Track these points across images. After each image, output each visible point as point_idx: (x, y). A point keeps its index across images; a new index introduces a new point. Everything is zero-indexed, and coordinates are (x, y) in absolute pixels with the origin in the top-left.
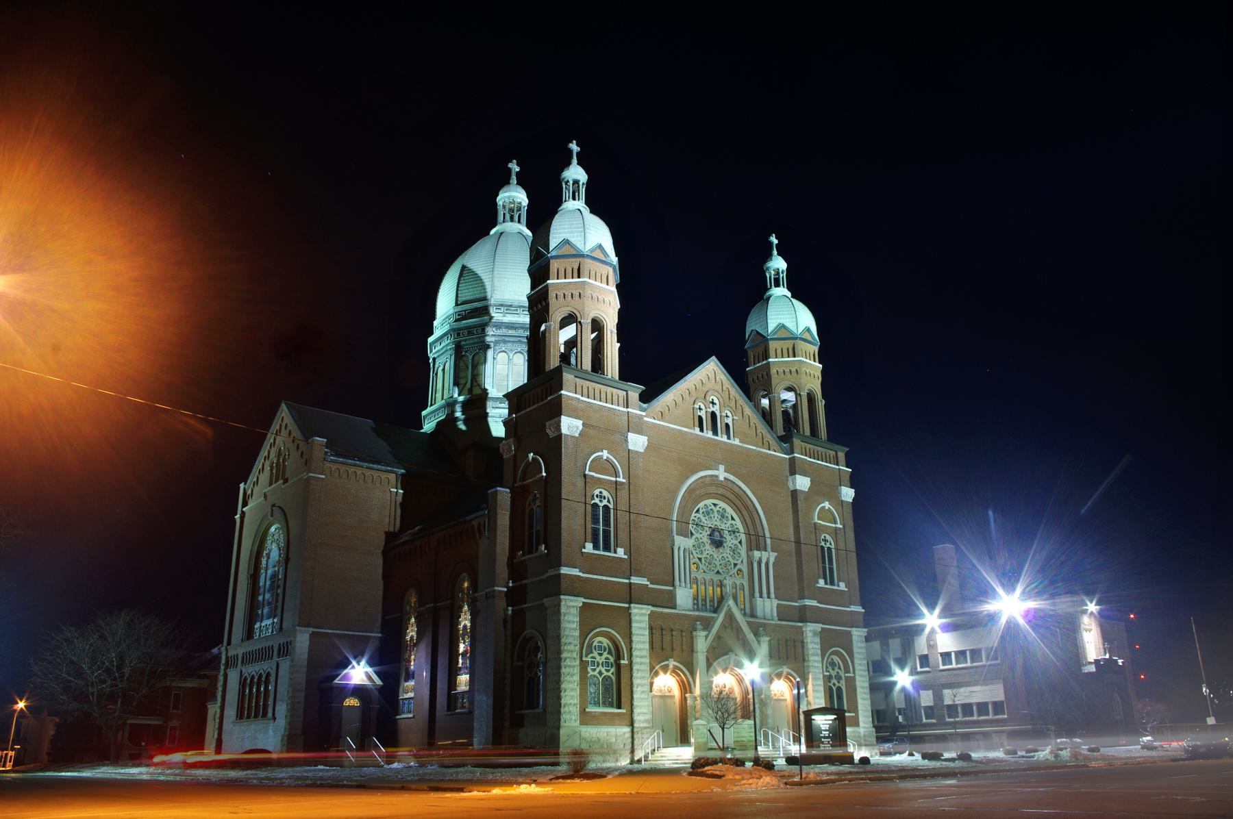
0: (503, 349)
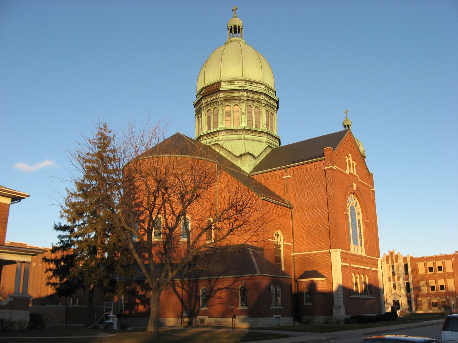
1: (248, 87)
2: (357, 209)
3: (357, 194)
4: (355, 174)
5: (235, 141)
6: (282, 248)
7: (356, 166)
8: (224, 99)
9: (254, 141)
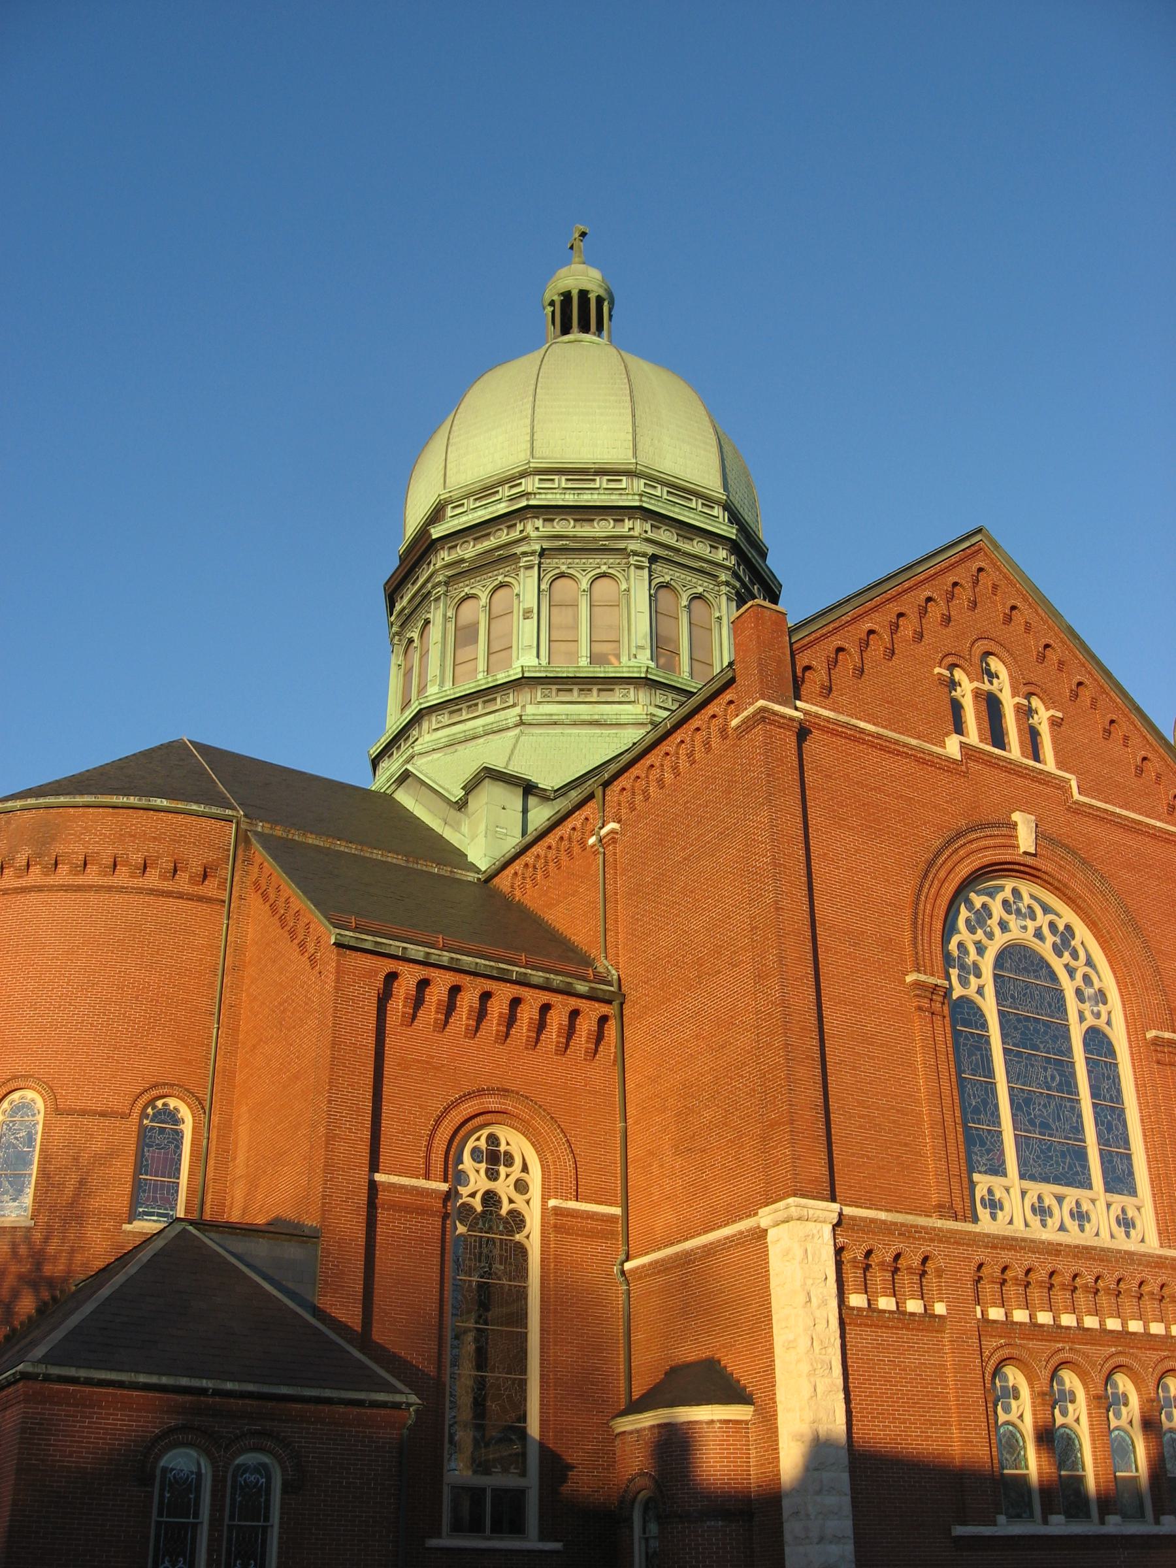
0: (604, 568)
1: (559, 494)
2: (1071, 972)
3: (1064, 876)
4: (1049, 763)
5: (481, 740)
6: (533, 1236)
7: (1055, 723)
8: (449, 573)
9: (575, 724)
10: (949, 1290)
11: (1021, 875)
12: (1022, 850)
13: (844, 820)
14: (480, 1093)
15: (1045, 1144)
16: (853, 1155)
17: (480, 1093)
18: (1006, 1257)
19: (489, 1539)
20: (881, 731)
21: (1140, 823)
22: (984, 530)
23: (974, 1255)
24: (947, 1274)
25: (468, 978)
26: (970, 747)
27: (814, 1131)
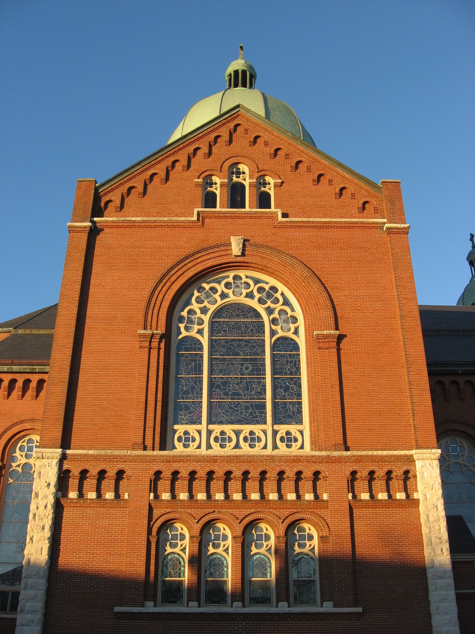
3: (265, 262)
10: (331, 487)
11: (237, 268)
12: (234, 254)
13: (114, 266)
14: (22, 422)
15: (234, 404)
16: (85, 424)
17: (22, 422)
18: (176, 466)
19: (8, 614)
20: (145, 219)
21: (329, 222)
22: (241, 106)
23: (153, 467)
24: (330, 479)
25: (18, 375)
26: (206, 212)
27: (56, 416)
